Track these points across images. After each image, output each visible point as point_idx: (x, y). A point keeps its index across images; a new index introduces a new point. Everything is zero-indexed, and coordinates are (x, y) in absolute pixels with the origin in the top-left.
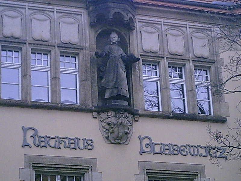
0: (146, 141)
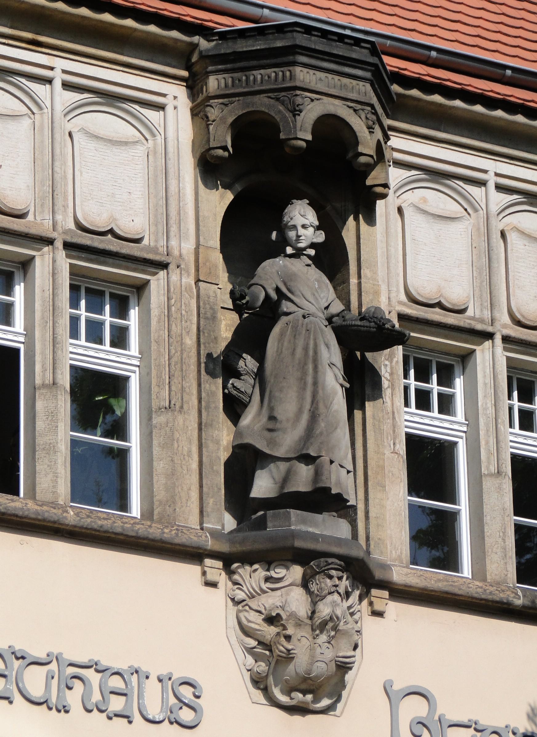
0: (415, 708)
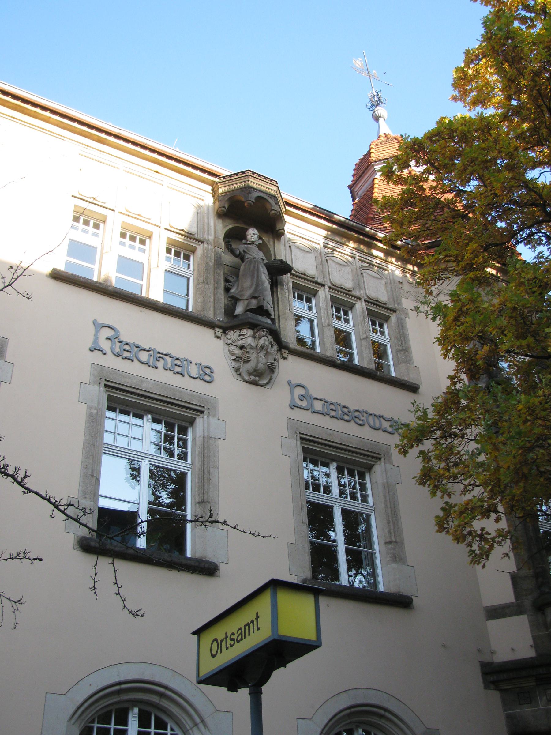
0: (299, 391)
